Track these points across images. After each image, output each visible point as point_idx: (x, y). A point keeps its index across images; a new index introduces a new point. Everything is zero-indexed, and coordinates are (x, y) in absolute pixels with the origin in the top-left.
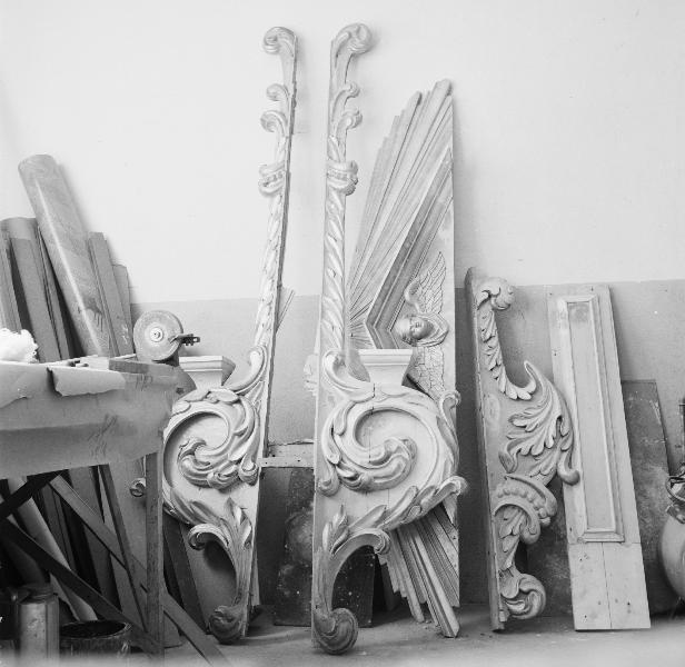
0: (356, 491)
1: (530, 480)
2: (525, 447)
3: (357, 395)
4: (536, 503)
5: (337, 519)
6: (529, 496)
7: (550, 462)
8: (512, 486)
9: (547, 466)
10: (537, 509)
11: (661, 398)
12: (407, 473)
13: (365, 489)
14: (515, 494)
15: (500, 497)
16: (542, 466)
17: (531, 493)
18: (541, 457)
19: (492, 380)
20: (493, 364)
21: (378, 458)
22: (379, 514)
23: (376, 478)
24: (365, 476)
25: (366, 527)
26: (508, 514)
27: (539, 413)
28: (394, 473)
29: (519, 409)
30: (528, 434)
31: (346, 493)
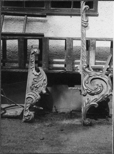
0: (90, 95)
1: (35, 92)
2: (35, 85)
3: (90, 74)
4: (36, 97)
5: (87, 101)
6: (34, 95)
7: (40, 89)
8: (31, 93)
9: (40, 90)
10: (36, 98)
11: (94, 62)
12: (101, 91)
13: (93, 95)
14: (31, 95)
15: (28, 95)
16: (39, 90)
17: (35, 95)
18: (39, 88)
19: (31, 70)
20: (32, 67)
21: (95, 88)
22: (96, 100)
23: (95, 92)
24: (93, 92)
25: (93, 102)
26: (29, 99)
27: (40, 79)
28: (99, 91)
29: (36, 77)
30: (37, 83)
31: (88, 95)
